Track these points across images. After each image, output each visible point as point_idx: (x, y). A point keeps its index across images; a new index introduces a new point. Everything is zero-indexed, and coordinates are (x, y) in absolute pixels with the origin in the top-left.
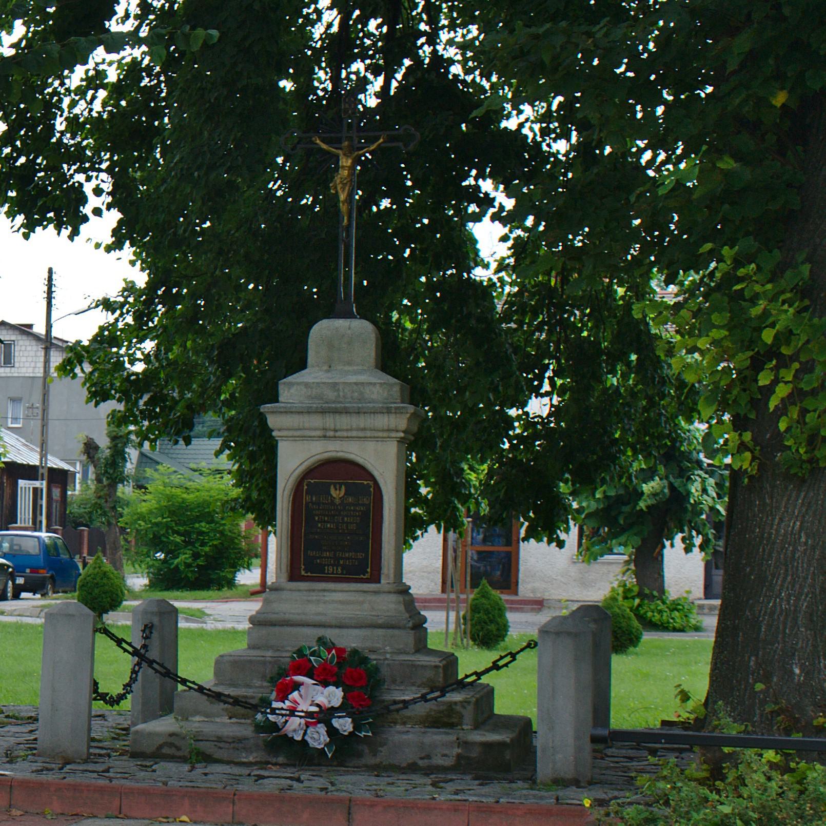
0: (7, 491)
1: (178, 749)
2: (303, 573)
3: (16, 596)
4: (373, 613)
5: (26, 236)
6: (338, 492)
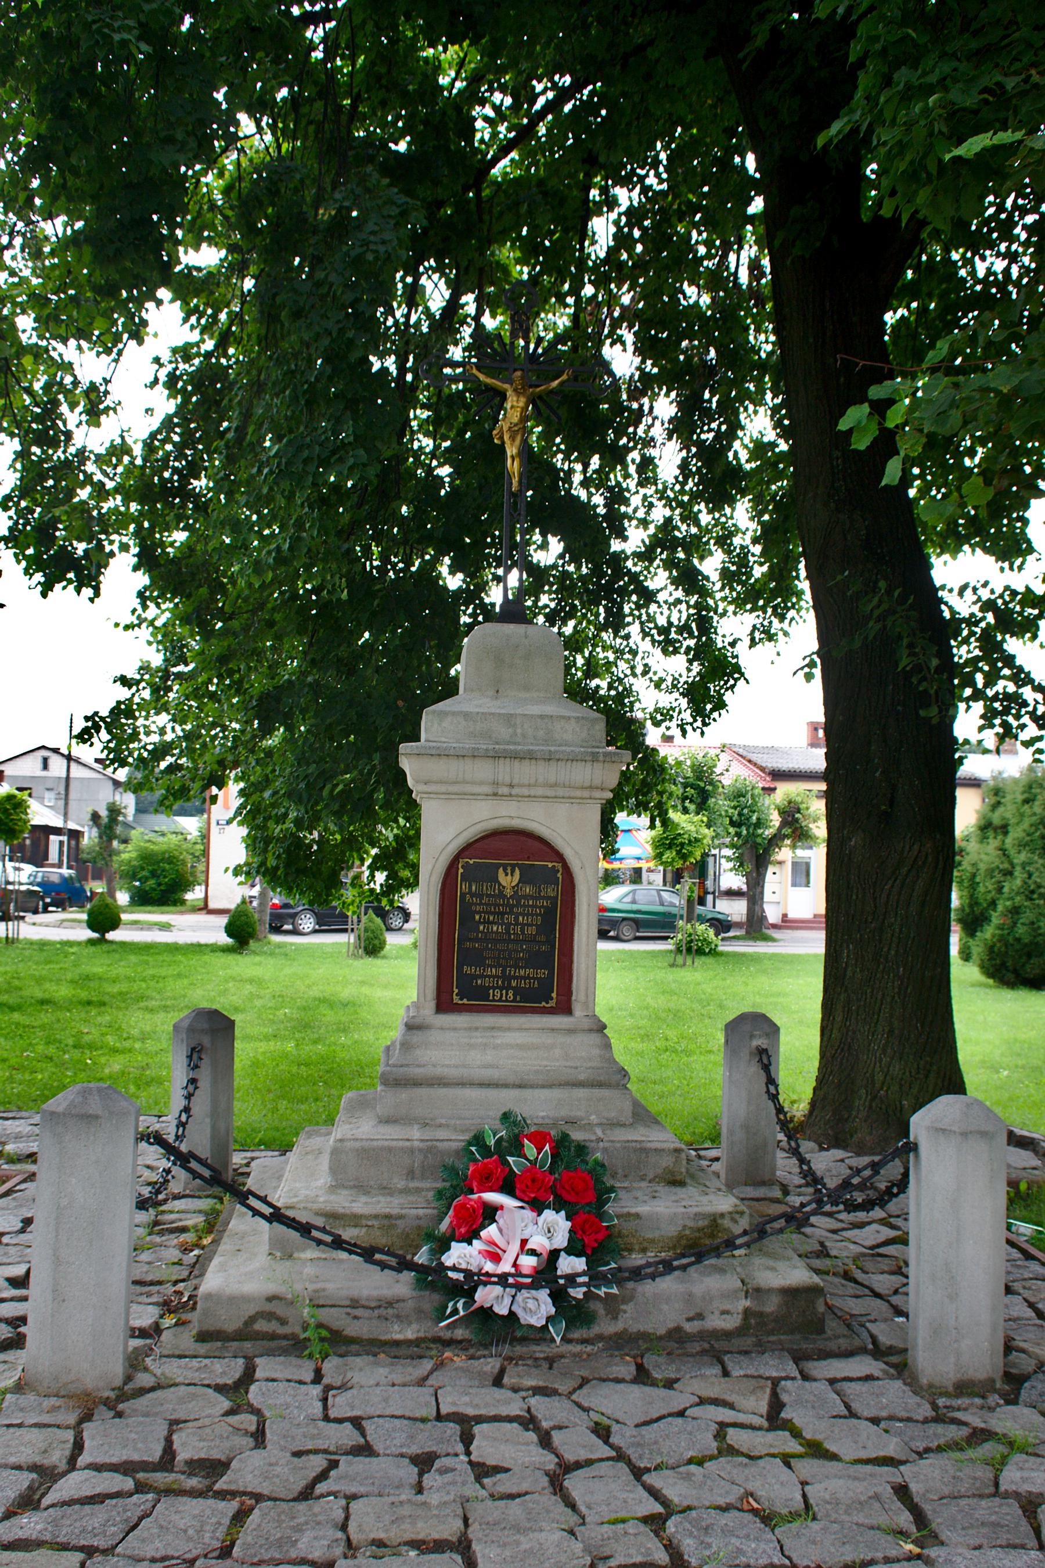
0: (43, 843)
1: (283, 1322)
2: (456, 999)
3: (45, 911)
4: (568, 1064)
5: (44, 595)
6: (509, 877)
